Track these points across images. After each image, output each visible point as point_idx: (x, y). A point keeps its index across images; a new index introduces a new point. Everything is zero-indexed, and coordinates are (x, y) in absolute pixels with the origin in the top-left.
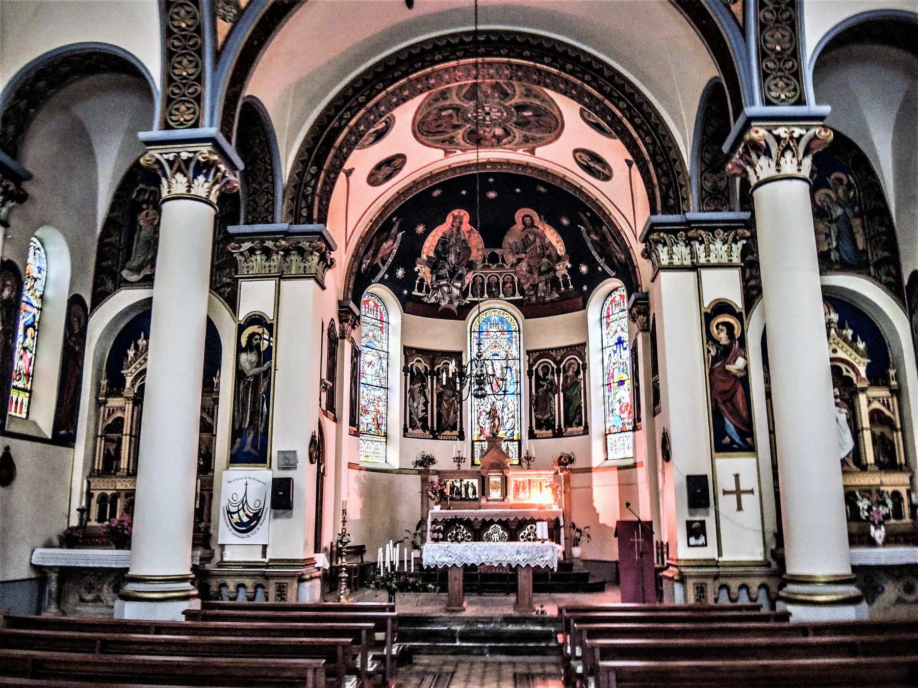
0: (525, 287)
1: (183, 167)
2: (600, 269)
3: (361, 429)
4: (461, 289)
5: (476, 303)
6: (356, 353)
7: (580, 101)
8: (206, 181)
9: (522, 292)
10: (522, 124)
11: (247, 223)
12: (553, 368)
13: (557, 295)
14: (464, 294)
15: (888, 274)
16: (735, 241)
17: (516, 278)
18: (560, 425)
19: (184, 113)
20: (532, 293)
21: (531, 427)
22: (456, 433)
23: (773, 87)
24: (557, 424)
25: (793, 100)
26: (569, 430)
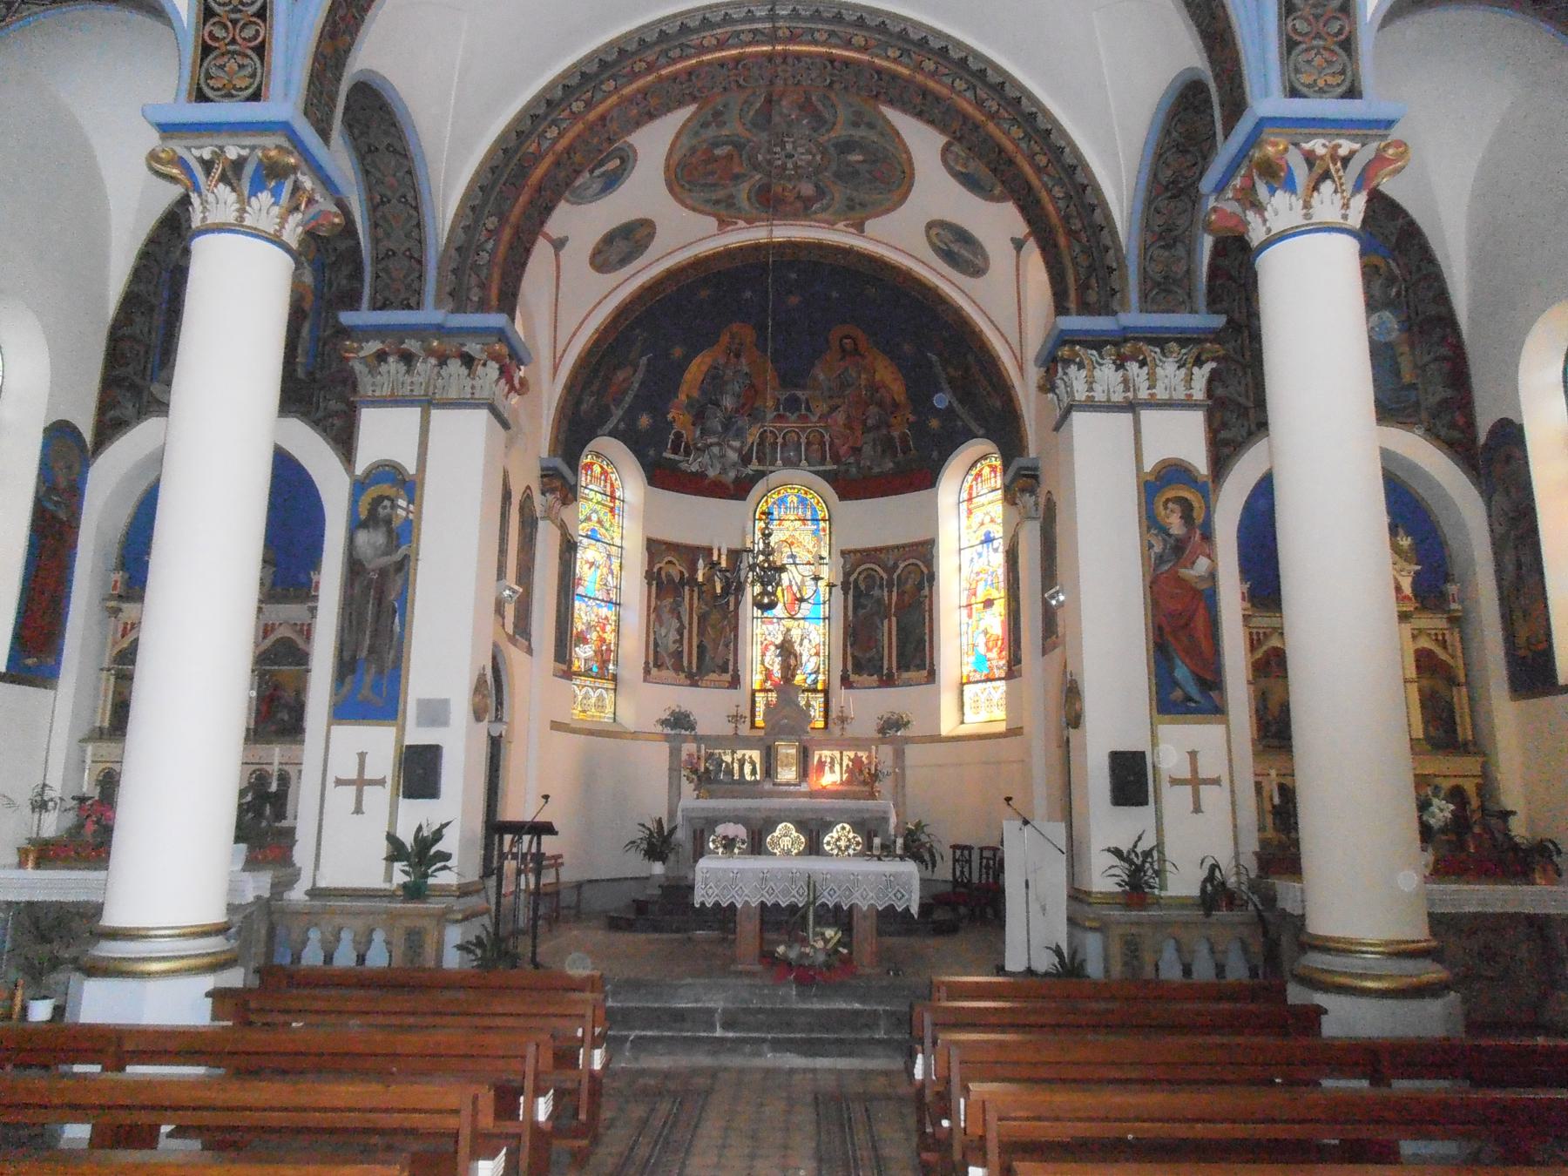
1: (229, 174)
2: (960, 423)
3: (575, 669)
4: (740, 451)
5: (762, 474)
6: (569, 548)
7: (943, 129)
8: (275, 204)
9: (836, 459)
10: (847, 175)
11: (375, 307)
14: (746, 460)
15: (1453, 425)
16: (1199, 362)
18: (890, 669)
19: (232, 70)
20: (851, 460)
21: (845, 670)
22: (727, 677)
23: (1304, 67)
25: (1340, 90)
26: (906, 675)
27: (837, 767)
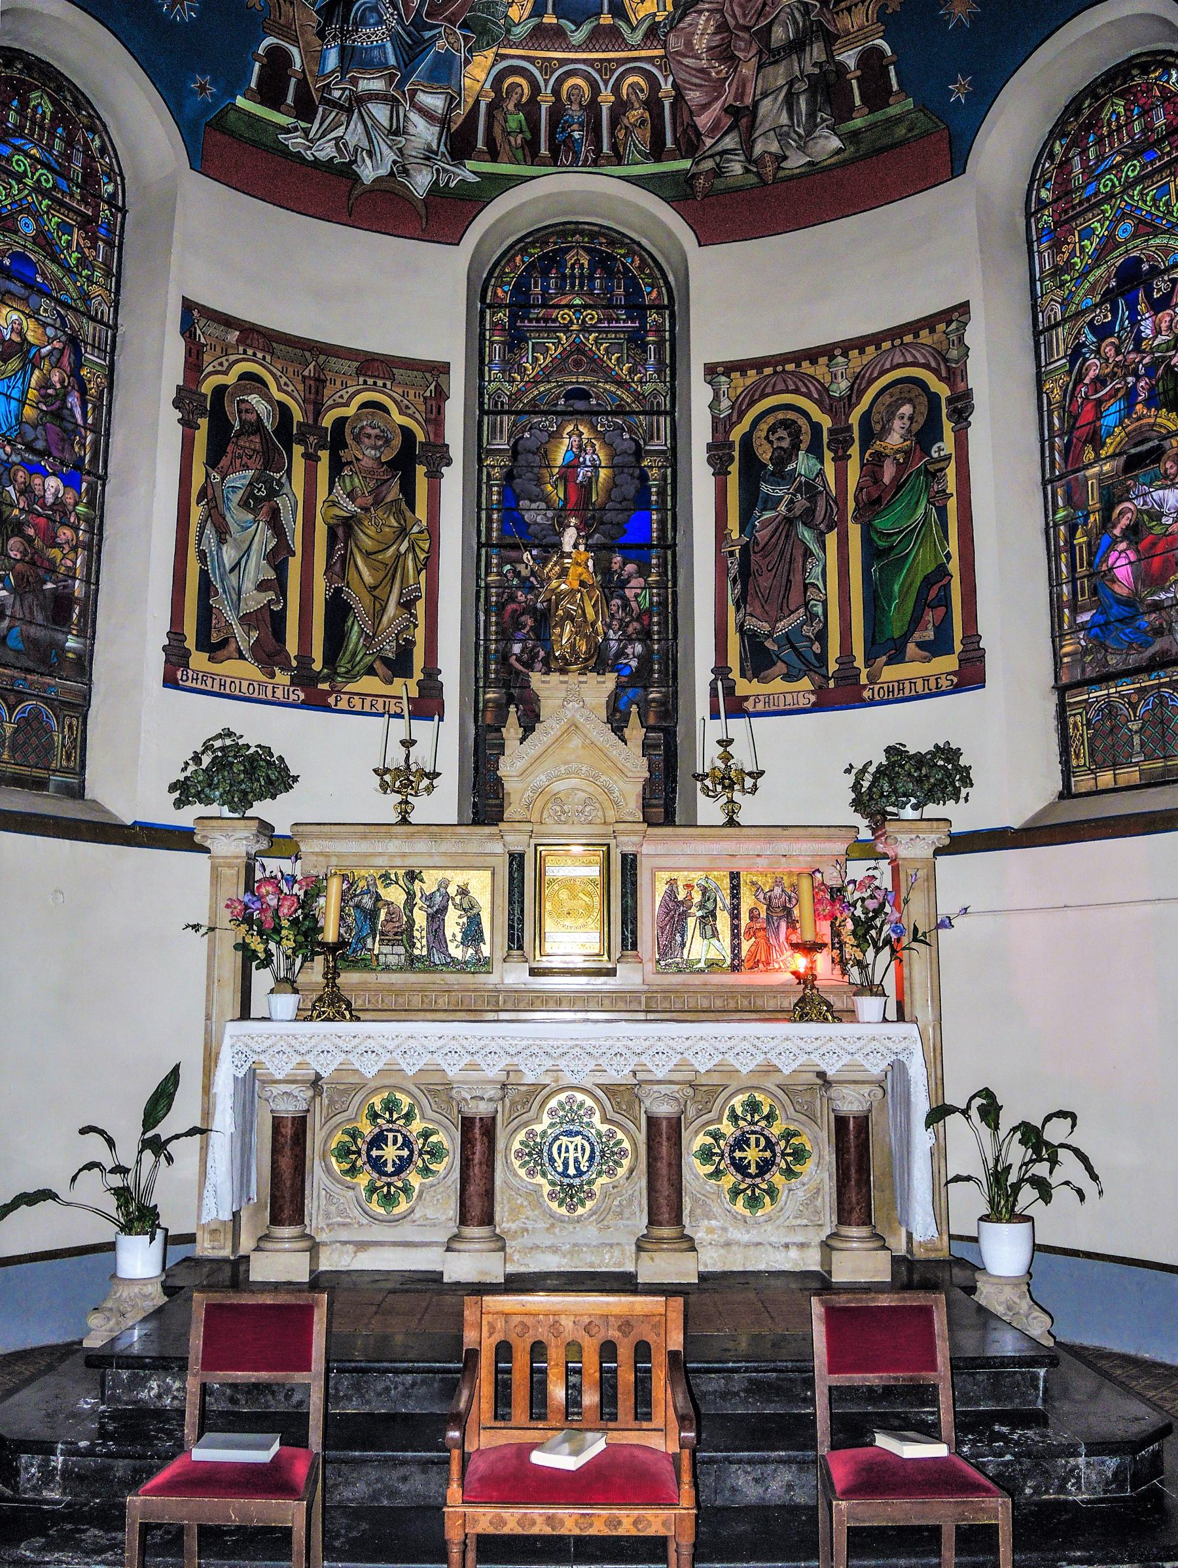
0: (704, 121)
4: (444, 122)
12: (816, 428)
13: (835, 143)
14: (460, 144)
17: (666, 86)
20: (730, 142)
22: (406, 688)
24: (834, 651)
26: (891, 673)
27: (723, 922)
